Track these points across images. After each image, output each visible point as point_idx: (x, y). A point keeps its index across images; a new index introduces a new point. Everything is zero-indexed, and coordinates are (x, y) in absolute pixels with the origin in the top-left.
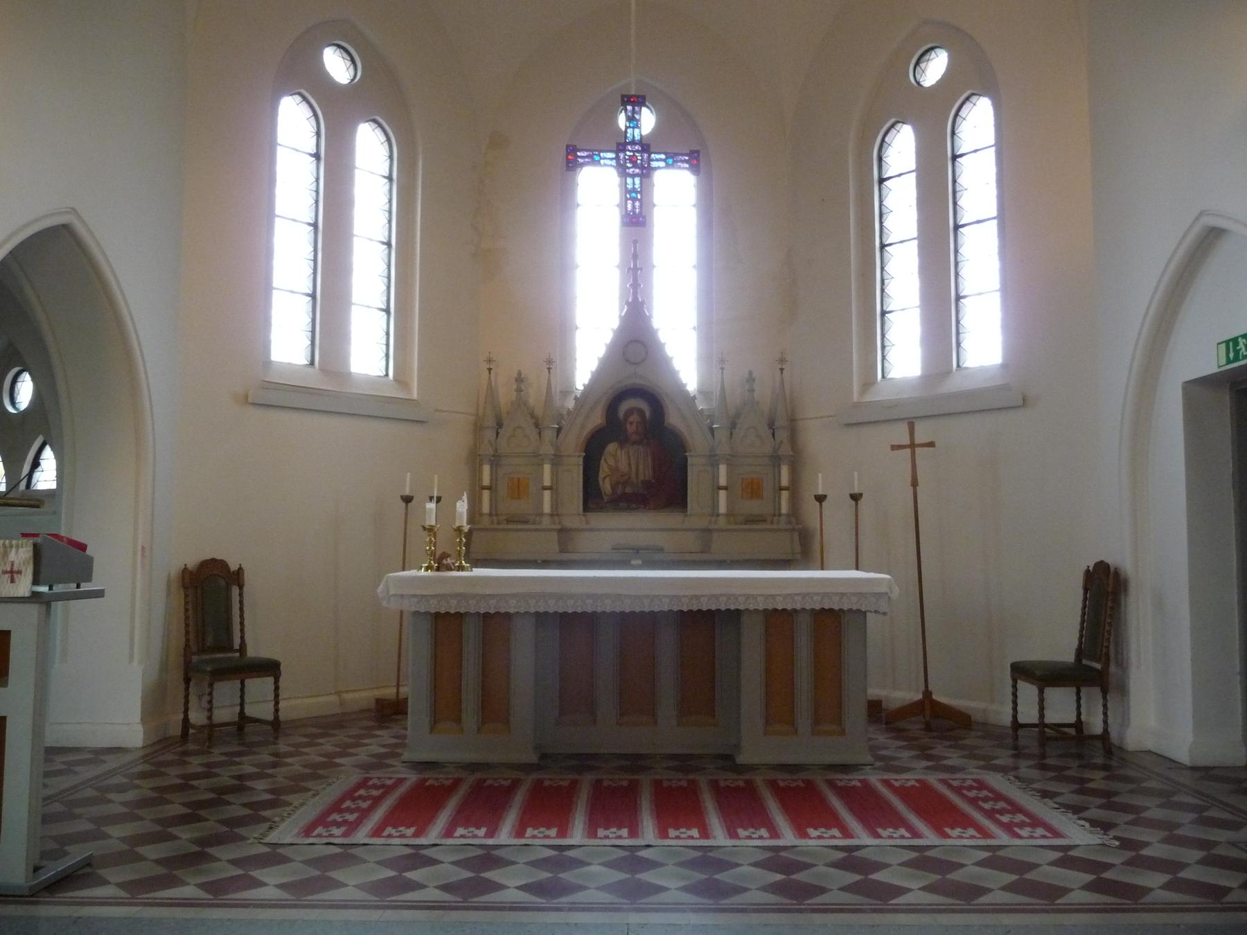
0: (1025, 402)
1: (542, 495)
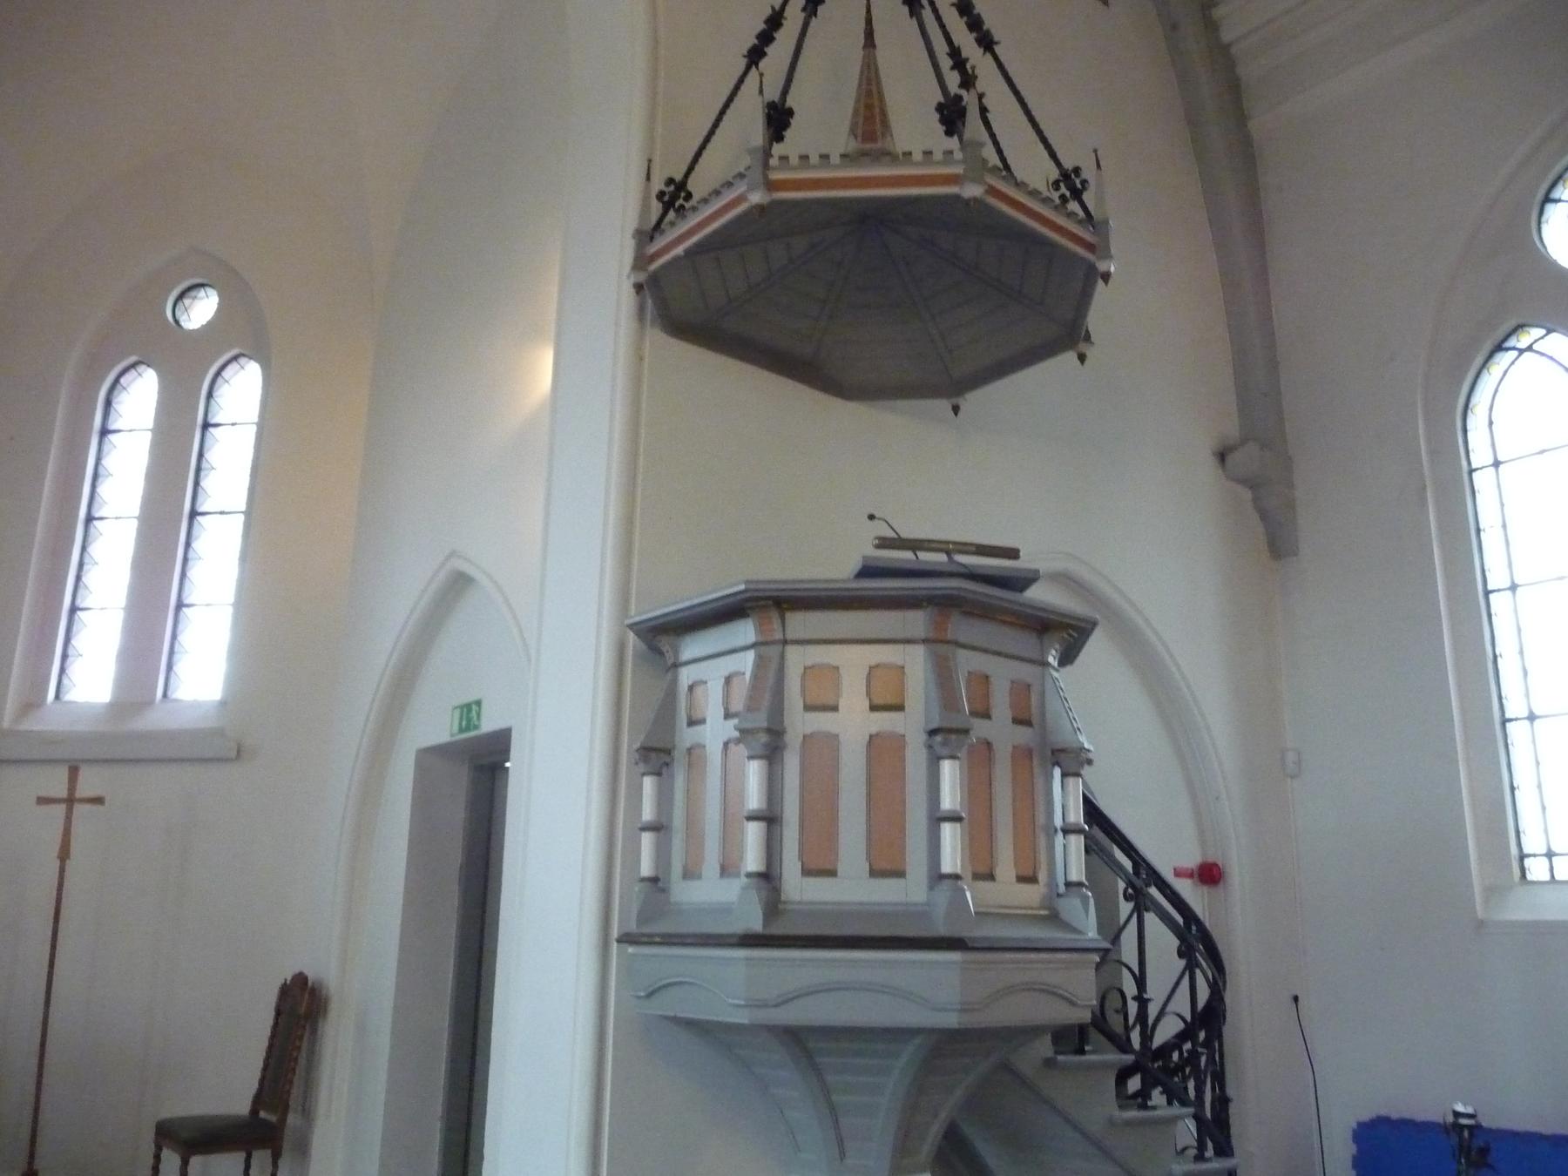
0: (239, 753)
1: (742, 831)
